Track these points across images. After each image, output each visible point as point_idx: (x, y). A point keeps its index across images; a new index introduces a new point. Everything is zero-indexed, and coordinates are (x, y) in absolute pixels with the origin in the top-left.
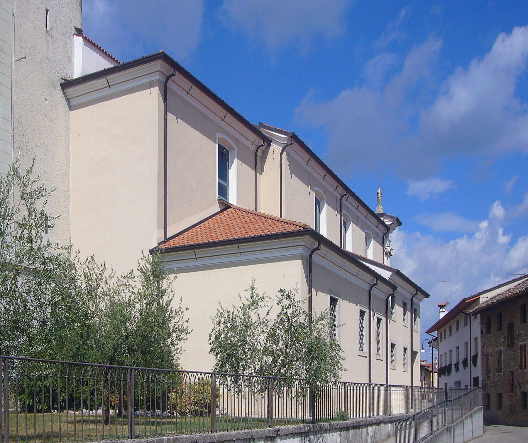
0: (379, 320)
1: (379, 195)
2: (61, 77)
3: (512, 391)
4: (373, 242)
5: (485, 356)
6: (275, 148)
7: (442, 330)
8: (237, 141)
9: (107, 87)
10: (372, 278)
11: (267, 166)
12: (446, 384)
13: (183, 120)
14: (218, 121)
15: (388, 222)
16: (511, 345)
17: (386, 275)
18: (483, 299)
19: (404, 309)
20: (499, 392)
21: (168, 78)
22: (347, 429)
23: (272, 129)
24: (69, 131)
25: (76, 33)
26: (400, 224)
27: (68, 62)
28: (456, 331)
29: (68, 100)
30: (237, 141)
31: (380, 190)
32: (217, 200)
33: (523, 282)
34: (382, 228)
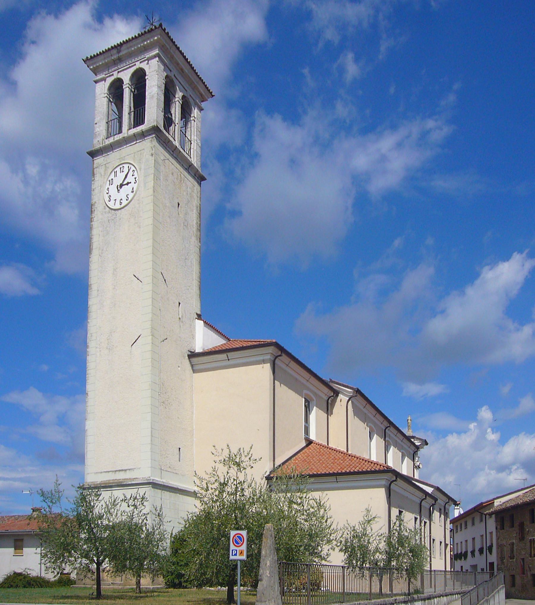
0: (425, 523)
1: (409, 421)
2: (188, 350)
3: (523, 573)
4: (407, 459)
5: (499, 546)
6: (342, 399)
7: (458, 524)
8: (315, 394)
9: (227, 360)
10: (422, 494)
11: (335, 410)
12: (462, 567)
13: (284, 385)
14: (304, 382)
15: (417, 443)
16: (522, 538)
17: (429, 490)
18: (497, 503)
19: (440, 513)
20: (512, 574)
21: (276, 357)
22: (424, 600)
23: (340, 385)
24: (193, 388)
25: (197, 317)
26: (427, 444)
27: (192, 338)
28: (472, 525)
29: (192, 366)
30: (315, 394)
31: (409, 418)
32: (304, 438)
33: (530, 490)
34: (413, 447)
